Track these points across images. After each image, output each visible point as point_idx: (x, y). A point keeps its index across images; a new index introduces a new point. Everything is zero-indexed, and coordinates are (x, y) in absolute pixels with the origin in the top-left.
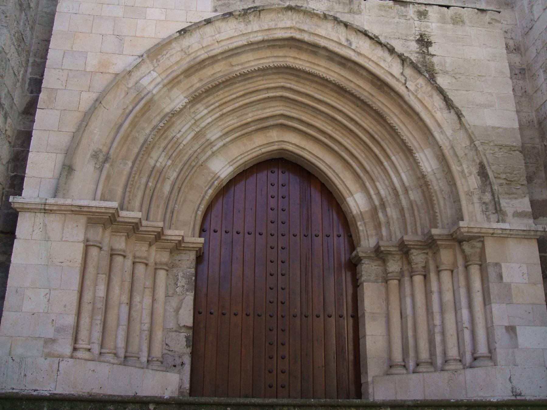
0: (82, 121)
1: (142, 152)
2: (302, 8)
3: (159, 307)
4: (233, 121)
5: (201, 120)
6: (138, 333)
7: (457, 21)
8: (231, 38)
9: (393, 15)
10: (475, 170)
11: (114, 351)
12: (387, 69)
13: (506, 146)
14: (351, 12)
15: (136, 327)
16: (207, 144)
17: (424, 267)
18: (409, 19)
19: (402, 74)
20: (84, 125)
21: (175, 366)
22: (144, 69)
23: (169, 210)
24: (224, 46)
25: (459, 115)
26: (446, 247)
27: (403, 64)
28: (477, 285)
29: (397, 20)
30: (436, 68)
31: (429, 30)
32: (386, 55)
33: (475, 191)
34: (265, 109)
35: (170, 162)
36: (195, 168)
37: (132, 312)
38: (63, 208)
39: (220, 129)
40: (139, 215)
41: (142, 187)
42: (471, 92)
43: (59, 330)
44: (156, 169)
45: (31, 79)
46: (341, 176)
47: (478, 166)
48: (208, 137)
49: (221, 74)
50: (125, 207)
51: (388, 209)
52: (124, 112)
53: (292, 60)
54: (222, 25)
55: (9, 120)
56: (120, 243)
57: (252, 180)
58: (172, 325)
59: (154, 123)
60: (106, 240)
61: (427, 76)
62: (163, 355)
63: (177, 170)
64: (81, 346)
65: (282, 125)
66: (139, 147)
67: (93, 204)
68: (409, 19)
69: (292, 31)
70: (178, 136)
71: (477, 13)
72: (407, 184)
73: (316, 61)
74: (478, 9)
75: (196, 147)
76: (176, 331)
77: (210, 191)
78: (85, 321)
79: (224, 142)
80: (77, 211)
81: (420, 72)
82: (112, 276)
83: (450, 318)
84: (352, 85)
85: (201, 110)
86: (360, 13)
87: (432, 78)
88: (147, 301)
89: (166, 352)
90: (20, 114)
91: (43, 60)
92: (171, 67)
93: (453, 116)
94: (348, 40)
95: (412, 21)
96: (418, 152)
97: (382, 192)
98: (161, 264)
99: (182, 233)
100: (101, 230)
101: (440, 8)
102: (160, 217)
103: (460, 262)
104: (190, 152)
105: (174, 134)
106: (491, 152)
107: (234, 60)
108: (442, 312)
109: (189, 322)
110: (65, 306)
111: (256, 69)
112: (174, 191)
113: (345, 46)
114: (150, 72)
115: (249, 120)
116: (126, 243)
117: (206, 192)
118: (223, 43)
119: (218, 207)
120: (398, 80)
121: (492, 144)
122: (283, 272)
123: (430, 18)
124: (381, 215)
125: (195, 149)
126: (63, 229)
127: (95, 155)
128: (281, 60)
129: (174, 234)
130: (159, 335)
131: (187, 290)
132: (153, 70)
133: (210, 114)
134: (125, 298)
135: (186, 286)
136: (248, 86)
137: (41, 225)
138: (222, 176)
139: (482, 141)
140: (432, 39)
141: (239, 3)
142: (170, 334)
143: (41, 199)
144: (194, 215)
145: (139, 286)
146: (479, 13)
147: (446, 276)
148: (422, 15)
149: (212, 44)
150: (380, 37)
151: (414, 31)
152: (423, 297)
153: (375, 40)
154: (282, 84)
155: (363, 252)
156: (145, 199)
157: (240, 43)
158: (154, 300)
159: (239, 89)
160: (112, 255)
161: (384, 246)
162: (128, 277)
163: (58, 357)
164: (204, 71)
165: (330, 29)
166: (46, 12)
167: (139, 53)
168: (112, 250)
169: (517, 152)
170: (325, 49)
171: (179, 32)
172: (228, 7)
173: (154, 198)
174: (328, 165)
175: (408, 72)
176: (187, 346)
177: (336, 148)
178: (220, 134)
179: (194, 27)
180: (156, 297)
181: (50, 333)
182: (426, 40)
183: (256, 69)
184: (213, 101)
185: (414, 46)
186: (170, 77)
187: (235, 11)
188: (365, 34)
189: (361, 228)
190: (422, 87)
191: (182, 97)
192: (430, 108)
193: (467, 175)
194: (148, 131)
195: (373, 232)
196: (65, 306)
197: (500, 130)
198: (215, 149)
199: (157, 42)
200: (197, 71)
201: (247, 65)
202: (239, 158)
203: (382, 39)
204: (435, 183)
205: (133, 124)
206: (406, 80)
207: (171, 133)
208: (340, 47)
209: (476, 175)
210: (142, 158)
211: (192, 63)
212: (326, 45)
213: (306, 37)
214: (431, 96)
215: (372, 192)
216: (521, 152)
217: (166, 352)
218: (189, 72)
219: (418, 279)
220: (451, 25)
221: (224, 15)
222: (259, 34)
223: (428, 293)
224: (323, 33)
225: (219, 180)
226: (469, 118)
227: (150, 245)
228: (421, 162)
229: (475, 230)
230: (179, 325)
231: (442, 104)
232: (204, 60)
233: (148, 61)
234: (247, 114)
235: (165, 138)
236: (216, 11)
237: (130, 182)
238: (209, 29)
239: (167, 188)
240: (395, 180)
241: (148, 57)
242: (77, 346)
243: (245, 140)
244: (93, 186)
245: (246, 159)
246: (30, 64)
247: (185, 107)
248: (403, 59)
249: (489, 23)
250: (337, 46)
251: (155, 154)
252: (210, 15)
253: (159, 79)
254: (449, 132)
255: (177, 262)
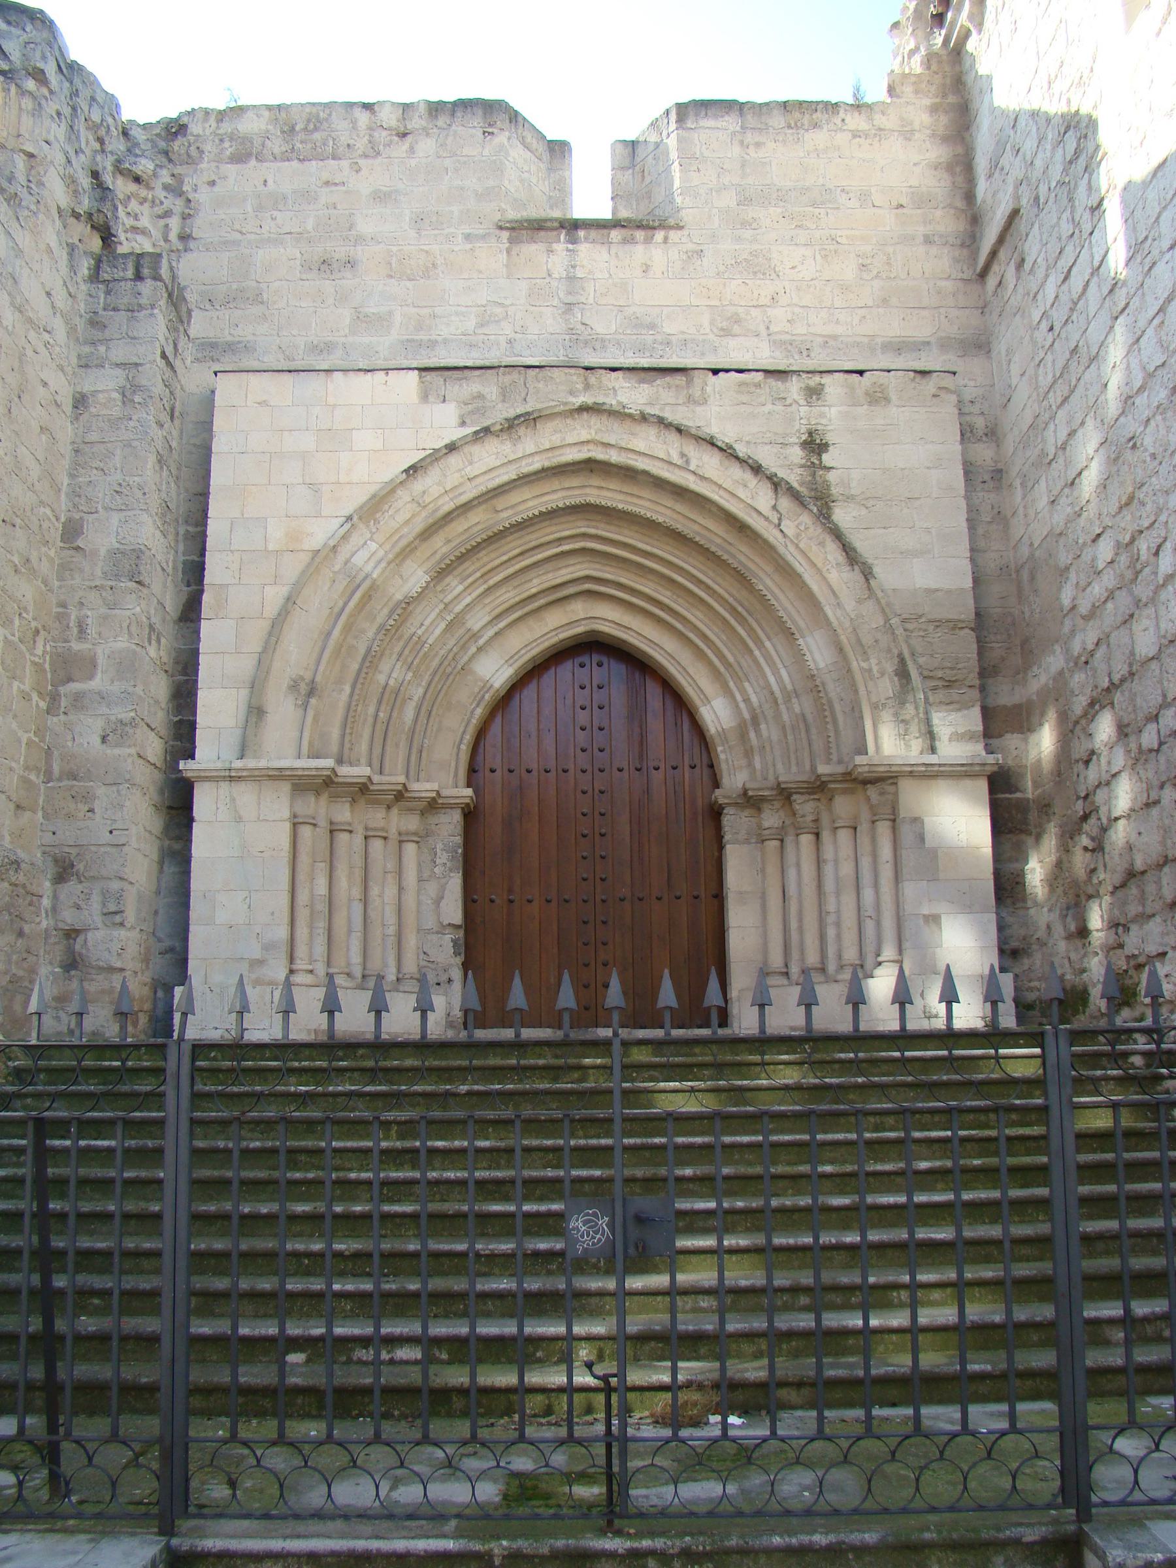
0: (270, 634)
1: (365, 670)
2: (605, 407)
3: (410, 900)
4: (508, 595)
5: (455, 602)
6: (380, 941)
7: (877, 398)
8: (490, 470)
9: (762, 399)
10: (890, 667)
11: (346, 970)
12: (749, 501)
13: (948, 621)
14: (690, 400)
15: (376, 932)
16: (467, 636)
17: (816, 821)
18: (790, 405)
19: (774, 507)
20: (274, 639)
21: (438, 984)
22: (356, 539)
23: (414, 751)
24: (480, 484)
25: (867, 574)
26: (845, 791)
27: (776, 490)
28: (886, 852)
29: (769, 407)
30: (834, 491)
31: (824, 421)
32: (748, 476)
33: (889, 701)
34: (560, 568)
35: (410, 674)
36: (451, 678)
37: (369, 911)
38: (256, 773)
39: (488, 609)
40: (367, 771)
41: (370, 720)
42: (891, 530)
43: (268, 947)
44: (388, 689)
45: (185, 563)
46: (691, 670)
47: (896, 660)
48: (469, 625)
49: (479, 527)
50: (345, 758)
51: (763, 726)
52: (331, 613)
53: (595, 492)
54: (476, 450)
55: (163, 640)
56: (343, 813)
57: (548, 678)
58: (430, 923)
59: (380, 620)
60: (322, 811)
61: (815, 510)
62: (420, 968)
63: (424, 684)
64: (300, 967)
65: (589, 593)
66: (360, 660)
67: (299, 764)
68: (790, 405)
69: (591, 447)
70: (420, 632)
71: (913, 380)
72: (789, 687)
73: (635, 491)
74: (915, 371)
75: (452, 642)
76: (437, 933)
77: (479, 711)
78: (302, 932)
79: (496, 629)
80: (277, 776)
81: (803, 504)
82: (335, 863)
83: (848, 900)
84: (696, 527)
85: (454, 585)
86: (705, 401)
87: (824, 515)
88: (391, 891)
89: (425, 963)
90: (175, 622)
91: (199, 529)
92: (397, 530)
93: (856, 576)
94: (683, 455)
95: (795, 406)
96: (803, 637)
97: (754, 699)
98: (407, 834)
99: (435, 786)
100: (313, 799)
101: (846, 376)
102: (400, 766)
103: (865, 816)
104: (442, 652)
105: (413, 630)
106: (922, 633)
107: (500, 503)
108: (838, 894)
109: (457, 917)
110: (273, 914)
111: (537, 513)
112: (420, 719)
113: (679, 467)
114: (365, 543)
115: (534, 591)
116: (352, 812)
117: (472, 712)
118: (478, 481)
119: (496, 728)
120: (767, 519)
121: (923, 620)
122: (603, 831)
123: (828, 398)
124: (752, 735)
125: (449, 647)
126: (259, 804)
127: (294, 686)
128: (577, 492)
129: (424, 788)
130: (411, 941)
131: (451, 870)
132: (371, 539)
133: (469, 591)
134: (357, 892)
135: (449, 864)
136: (528, 538)
137: (228, 800)
138: (497, 685)
139: (904, 616)
140: (830, 438)
141: (500, 405)
142: (429, 937)
143: (224, 761)
144: (455, 750)
145: (376, 870)
146: (918, 377)
147: (844, 836)
148: (815, 393)
149: (461, 484)
150: (737, 446)
151: (797, 427)
152: (813, 868)
153: (728, 452)
154: (583, 530)
155: (724, 797)
156: (375, 740)
157: (505, 478)
158: (401, 889)
159: (511, 545)
160: (331, 832)
161: (753, 789)
162: (358, 861)
163: (269, 984)
164: (453, 524)
165: (653, 438)
166: (195, 445)
167: (347, 513)
168: (331, 823)
169: (967, 631)
170: (646, 473)
171: (406, 471)
172: (483, 414)
173: (390, 734)
174: (669, 654)
175: (785, 503)
176: (456, 954)
177: (679, 626)
178: (487, 618)
179: (429, 460)
180: (404, 884)
181: (257, 954)
182: (818, 441)
183: (537, 513)
184: (471, 569)
185: (797, 454)
186: (397, 549)
187: (493, 424)
188: (711, 443)
189: (722, 756)
190: (806, 528)
191: (420, 573)
192: (820, 565)
193: (877, 675)
194: (370, 634)
195: (744, 762)
196: (273, 914)
197: (939, 594)
198: (481, 642)
199: (373, 489)
200: (441, 527)
201: (522, 507)
202: (523, 652)
203: (741, 449)
204: (830, 686)
205: (348, 628)
206: (780, 519)
207: (410, 628)
208: (671, 468)
209: (893, 674)
210: (363, 684)
211: (431, 521)
212: (647, 468)
213: (614, 457)
214: (822, 544)
215: (739, 697)
216: (972, 629)
217: (425, 963)
218: (427, 534)
219: (806, 839)
220: (865, 407)
221: (476, 433)
222: (537, 458)
223: (819, 862)
224: (639, 444)
225: (492, 692)
226: (885, 575)
227: (389, 807)
228: (808, 654)
229: (882, 769)
230: (441, 923)
231: (840, 557)
232: (450, 513)
233: (361, 525)
234: (531, 580)
235: (399, 639)
236: (463, 424)
237: (350, 719)
238: (454, 460)
239: (409, 713)
240: (772, 679)
241: (360, 518)
242: (294, 967)
243: (531, 622)
244: (297, 734)
245: (534, 652)
246: (181, 538)
247: (424, 589)
248: (776, 484)
249: (934, 396)
250: (666, 466)
251: (385, 666)
252: (457, 434)
253: (381, 553)
254: (850, 605)
255: (433, 827)
